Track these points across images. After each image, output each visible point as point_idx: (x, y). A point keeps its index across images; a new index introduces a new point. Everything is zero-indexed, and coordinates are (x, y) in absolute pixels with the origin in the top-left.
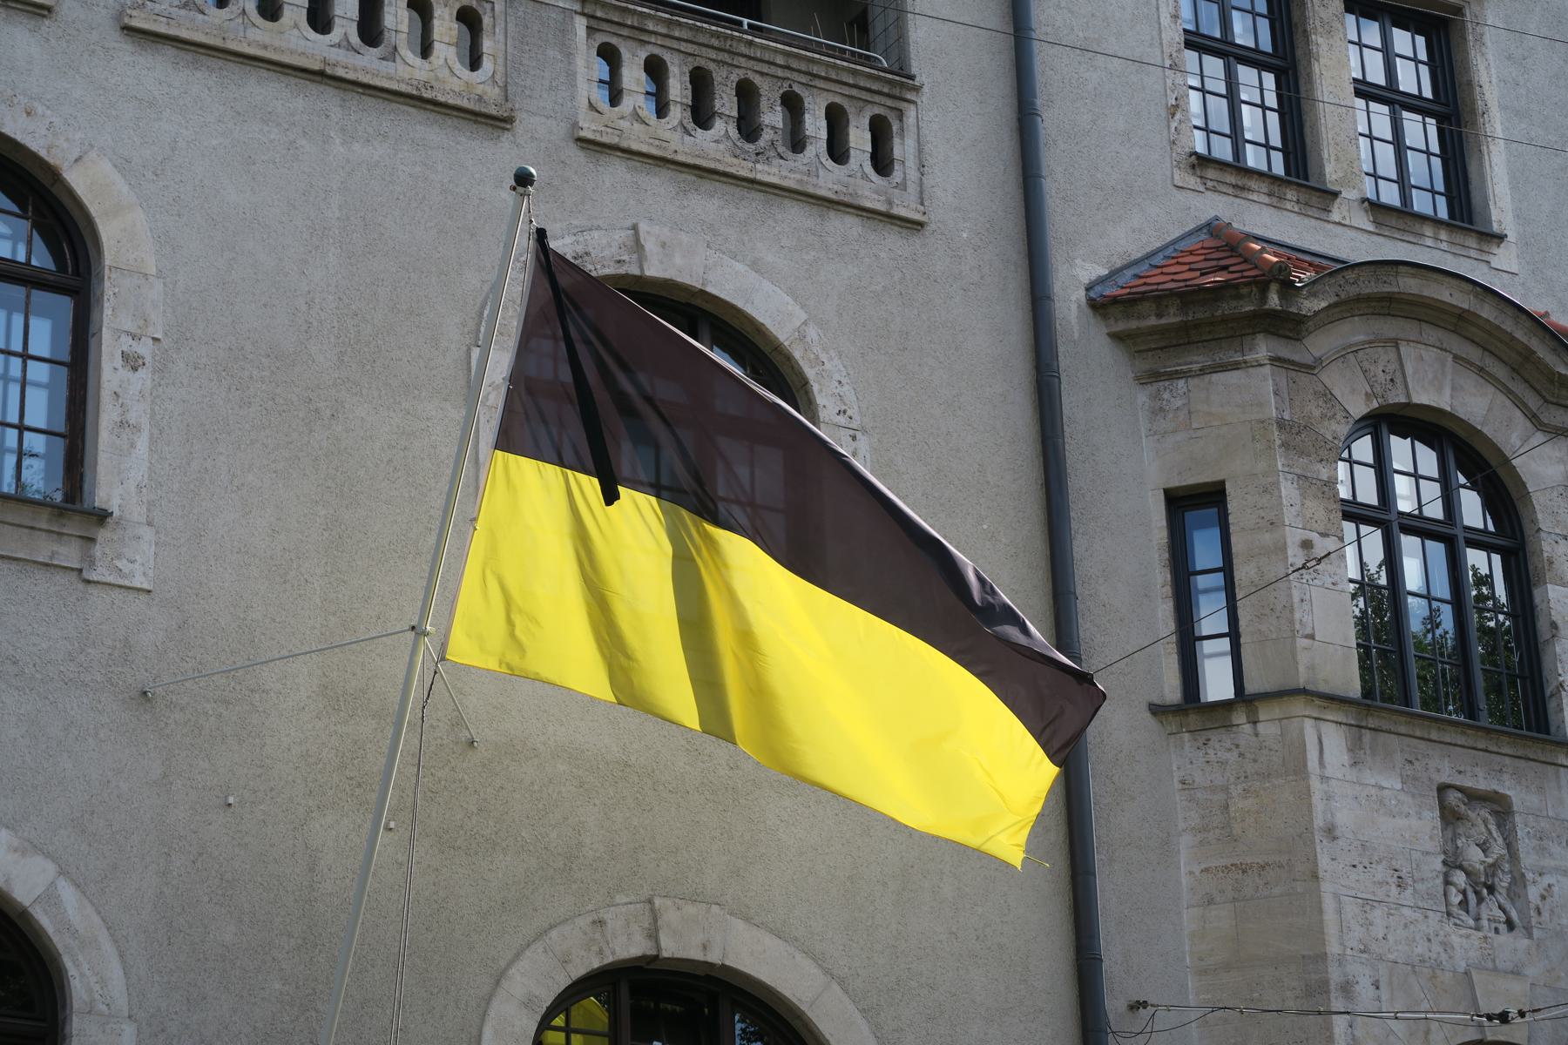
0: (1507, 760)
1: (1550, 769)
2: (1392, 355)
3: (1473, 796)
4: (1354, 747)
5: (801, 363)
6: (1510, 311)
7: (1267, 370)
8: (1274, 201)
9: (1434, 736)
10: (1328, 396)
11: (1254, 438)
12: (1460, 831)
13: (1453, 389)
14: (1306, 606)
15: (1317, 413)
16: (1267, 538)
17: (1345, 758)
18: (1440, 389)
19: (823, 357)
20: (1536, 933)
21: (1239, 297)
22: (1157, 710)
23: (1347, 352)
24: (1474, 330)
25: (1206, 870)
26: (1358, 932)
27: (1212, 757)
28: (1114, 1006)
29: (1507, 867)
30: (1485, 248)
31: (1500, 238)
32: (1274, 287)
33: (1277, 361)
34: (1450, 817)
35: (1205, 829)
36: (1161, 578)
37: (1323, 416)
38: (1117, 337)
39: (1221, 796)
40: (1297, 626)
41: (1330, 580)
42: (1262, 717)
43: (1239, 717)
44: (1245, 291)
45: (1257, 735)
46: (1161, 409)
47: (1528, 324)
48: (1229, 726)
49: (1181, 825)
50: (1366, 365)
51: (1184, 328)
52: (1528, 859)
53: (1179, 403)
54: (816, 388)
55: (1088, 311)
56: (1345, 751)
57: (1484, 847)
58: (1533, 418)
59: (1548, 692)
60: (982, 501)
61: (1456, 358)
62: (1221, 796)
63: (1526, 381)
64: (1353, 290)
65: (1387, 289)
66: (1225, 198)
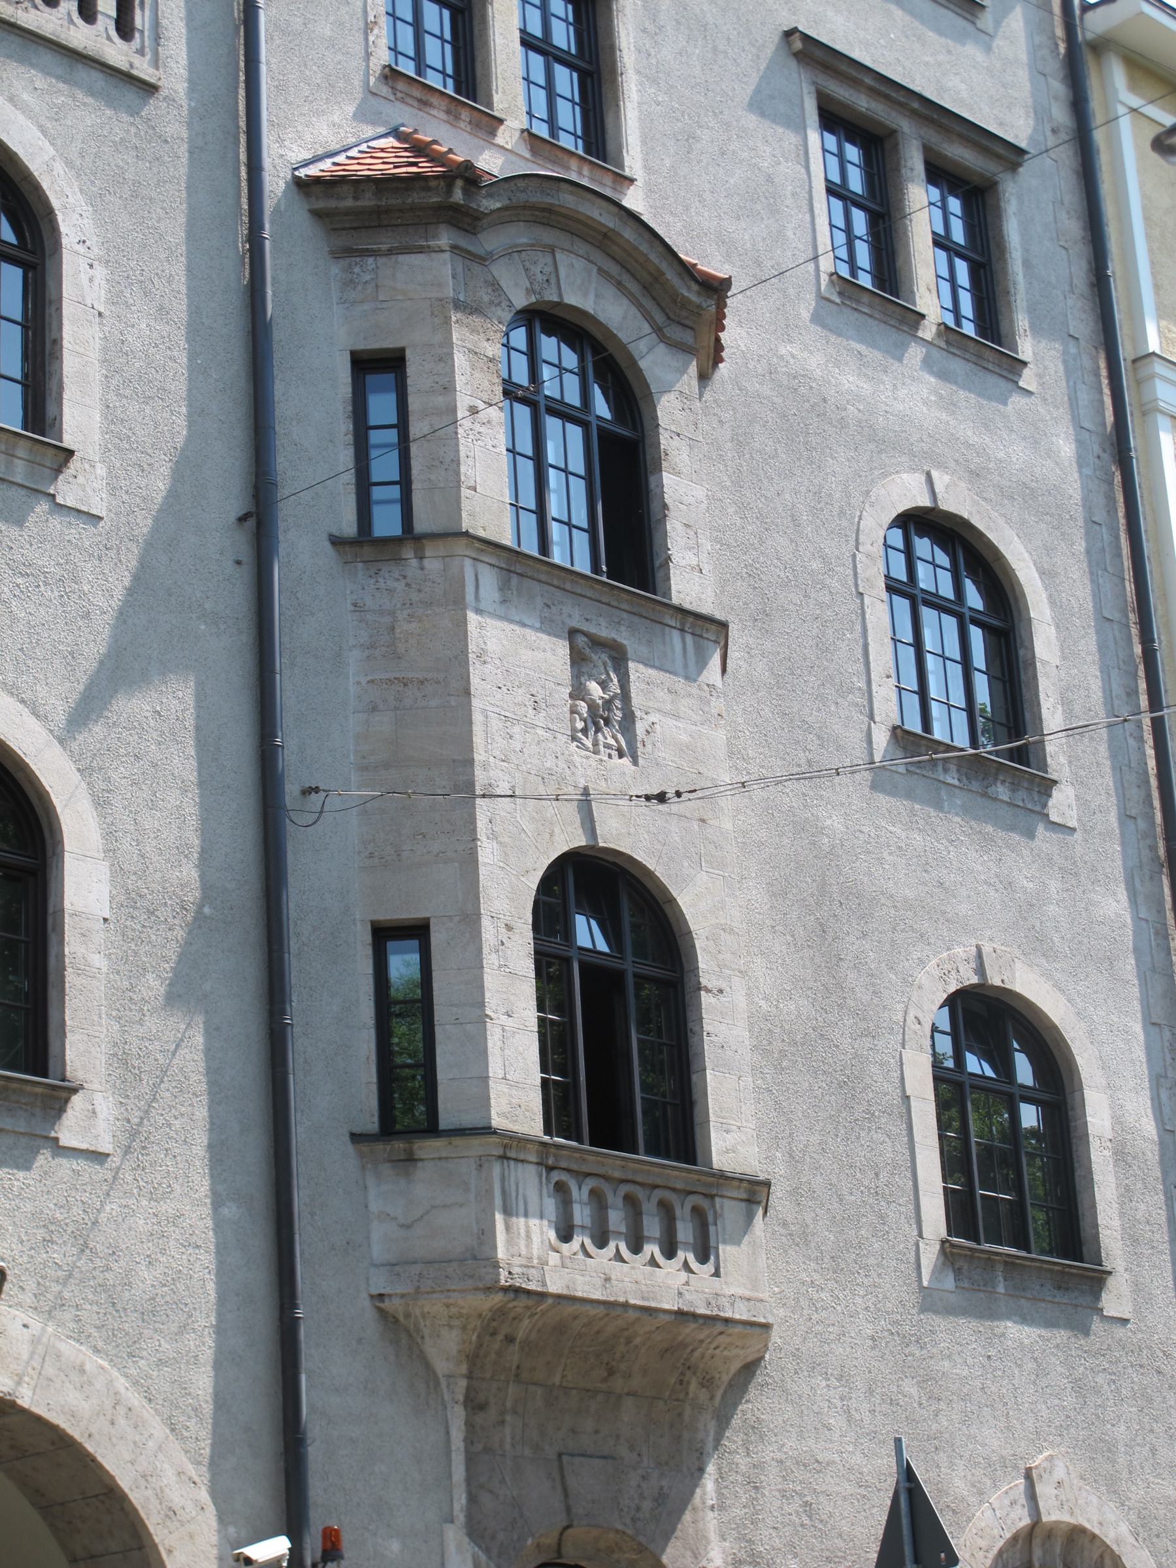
0: (625, 615)
1: (658, 626)
2: (549, 259)
3: (597, 643)
4: (504, 587)
5: (48, 193)
6: (647, 235)
7: (447, 256)
8: (451, 118)
9: (568, 586)
10: (495, 286)
11: (432, 314)
12: (584, 670)
13: (597, 296)
14: (470, 461)
15: (486, 299)
16: (440, 400)
17: (496, 596)
18: (585, 294)
19: (68, 191)
20: (641, 761)
21: (428, 189)
22: (337, 542)
23: (512, 252)
24: (615, 248)
25: (372, 681)
26: (501, 742)
27: (382, 585)
28: (291, 790)
29: (618, 703)
30: (618, 188)
31: (632, 181)
32: (459, 183)
33: (455, 248)
34: (578, 659)
35: (372, 646)
36: (344, 428)
37: (491, 302)
38: (317, 214)
39: (387, 620)
40: (463, 478)
41: (490, 443)
42: (428, 554)
43: (408, 553)
44: (433, 184)
45: (422, 569)
46: (351, 281)
47: (661, 249)
48: (398, 560)
49: (352, 642)
50: (527, 264)
51: (378, 212)
52: (637, 700)
53: (367, 277)
54: (60, 218)
55: (294, 188)
56: (496, 588)
57: (604, 685)
58: (658, 330)
59: (657, 563)
60: (198, 338)
61: (600, 270)
62: (387, 620)
63: (654, 299)
64: (523, 197)
65: (549, 200)
66: (410, 109)
